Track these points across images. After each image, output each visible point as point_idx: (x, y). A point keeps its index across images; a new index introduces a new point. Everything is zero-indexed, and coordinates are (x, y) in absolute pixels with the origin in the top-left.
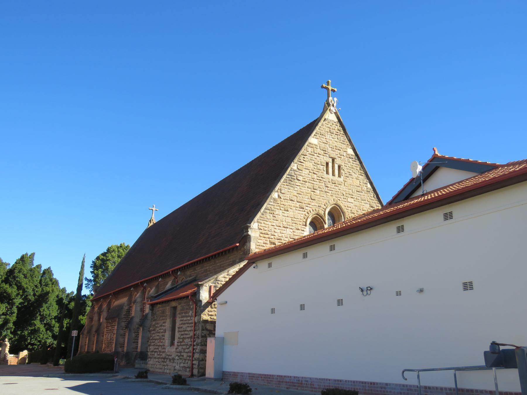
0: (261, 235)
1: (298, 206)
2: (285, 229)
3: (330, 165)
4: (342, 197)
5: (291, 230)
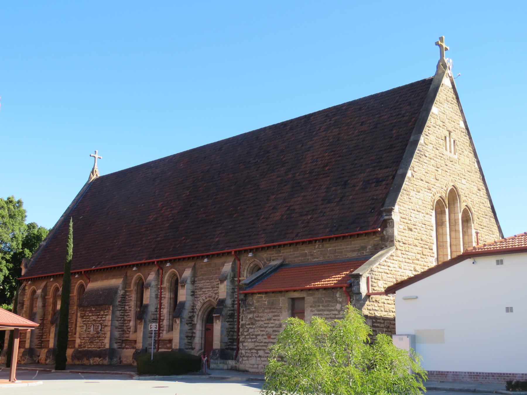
0: (402, 220)
1: (426, 186)
2: (418, 213)
3: (448, 138)
4: (458, 177)
5: (423, 215)
